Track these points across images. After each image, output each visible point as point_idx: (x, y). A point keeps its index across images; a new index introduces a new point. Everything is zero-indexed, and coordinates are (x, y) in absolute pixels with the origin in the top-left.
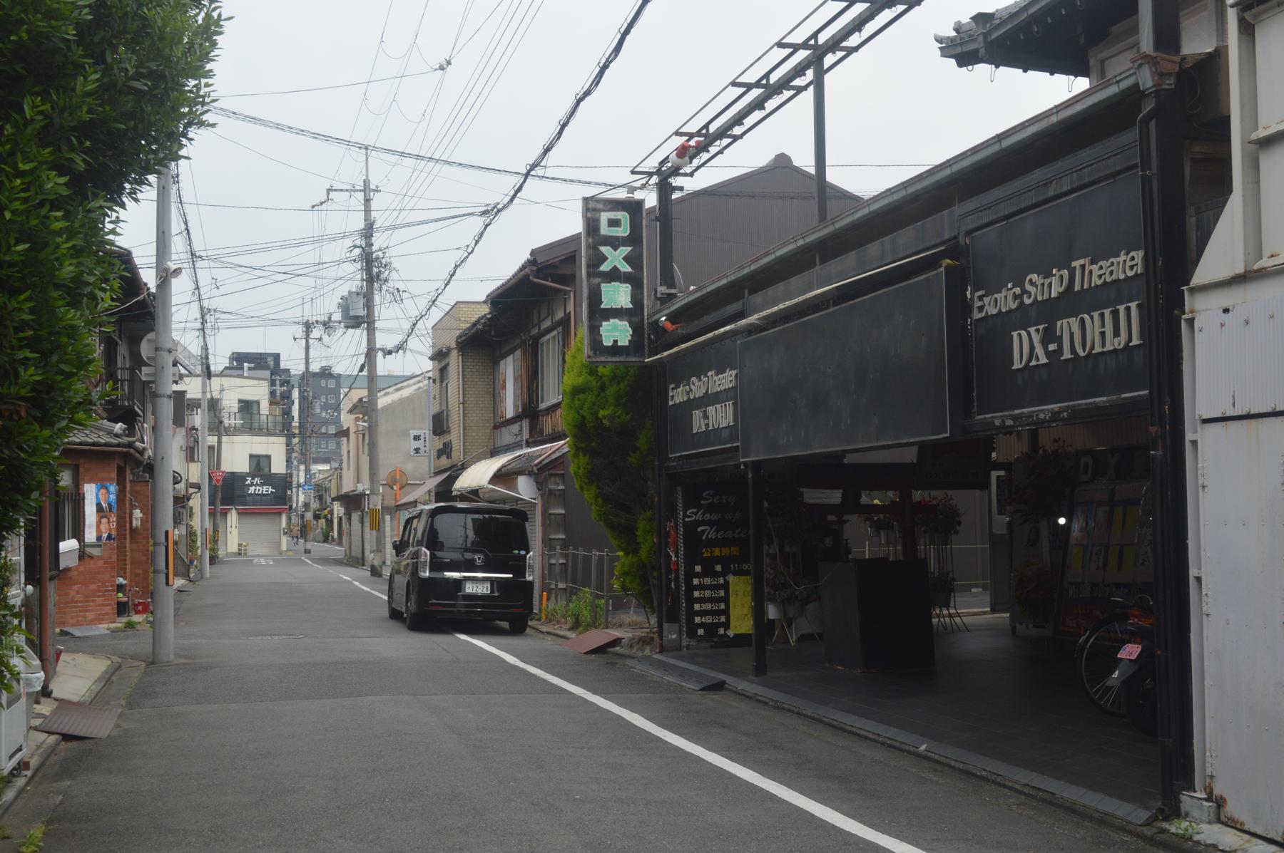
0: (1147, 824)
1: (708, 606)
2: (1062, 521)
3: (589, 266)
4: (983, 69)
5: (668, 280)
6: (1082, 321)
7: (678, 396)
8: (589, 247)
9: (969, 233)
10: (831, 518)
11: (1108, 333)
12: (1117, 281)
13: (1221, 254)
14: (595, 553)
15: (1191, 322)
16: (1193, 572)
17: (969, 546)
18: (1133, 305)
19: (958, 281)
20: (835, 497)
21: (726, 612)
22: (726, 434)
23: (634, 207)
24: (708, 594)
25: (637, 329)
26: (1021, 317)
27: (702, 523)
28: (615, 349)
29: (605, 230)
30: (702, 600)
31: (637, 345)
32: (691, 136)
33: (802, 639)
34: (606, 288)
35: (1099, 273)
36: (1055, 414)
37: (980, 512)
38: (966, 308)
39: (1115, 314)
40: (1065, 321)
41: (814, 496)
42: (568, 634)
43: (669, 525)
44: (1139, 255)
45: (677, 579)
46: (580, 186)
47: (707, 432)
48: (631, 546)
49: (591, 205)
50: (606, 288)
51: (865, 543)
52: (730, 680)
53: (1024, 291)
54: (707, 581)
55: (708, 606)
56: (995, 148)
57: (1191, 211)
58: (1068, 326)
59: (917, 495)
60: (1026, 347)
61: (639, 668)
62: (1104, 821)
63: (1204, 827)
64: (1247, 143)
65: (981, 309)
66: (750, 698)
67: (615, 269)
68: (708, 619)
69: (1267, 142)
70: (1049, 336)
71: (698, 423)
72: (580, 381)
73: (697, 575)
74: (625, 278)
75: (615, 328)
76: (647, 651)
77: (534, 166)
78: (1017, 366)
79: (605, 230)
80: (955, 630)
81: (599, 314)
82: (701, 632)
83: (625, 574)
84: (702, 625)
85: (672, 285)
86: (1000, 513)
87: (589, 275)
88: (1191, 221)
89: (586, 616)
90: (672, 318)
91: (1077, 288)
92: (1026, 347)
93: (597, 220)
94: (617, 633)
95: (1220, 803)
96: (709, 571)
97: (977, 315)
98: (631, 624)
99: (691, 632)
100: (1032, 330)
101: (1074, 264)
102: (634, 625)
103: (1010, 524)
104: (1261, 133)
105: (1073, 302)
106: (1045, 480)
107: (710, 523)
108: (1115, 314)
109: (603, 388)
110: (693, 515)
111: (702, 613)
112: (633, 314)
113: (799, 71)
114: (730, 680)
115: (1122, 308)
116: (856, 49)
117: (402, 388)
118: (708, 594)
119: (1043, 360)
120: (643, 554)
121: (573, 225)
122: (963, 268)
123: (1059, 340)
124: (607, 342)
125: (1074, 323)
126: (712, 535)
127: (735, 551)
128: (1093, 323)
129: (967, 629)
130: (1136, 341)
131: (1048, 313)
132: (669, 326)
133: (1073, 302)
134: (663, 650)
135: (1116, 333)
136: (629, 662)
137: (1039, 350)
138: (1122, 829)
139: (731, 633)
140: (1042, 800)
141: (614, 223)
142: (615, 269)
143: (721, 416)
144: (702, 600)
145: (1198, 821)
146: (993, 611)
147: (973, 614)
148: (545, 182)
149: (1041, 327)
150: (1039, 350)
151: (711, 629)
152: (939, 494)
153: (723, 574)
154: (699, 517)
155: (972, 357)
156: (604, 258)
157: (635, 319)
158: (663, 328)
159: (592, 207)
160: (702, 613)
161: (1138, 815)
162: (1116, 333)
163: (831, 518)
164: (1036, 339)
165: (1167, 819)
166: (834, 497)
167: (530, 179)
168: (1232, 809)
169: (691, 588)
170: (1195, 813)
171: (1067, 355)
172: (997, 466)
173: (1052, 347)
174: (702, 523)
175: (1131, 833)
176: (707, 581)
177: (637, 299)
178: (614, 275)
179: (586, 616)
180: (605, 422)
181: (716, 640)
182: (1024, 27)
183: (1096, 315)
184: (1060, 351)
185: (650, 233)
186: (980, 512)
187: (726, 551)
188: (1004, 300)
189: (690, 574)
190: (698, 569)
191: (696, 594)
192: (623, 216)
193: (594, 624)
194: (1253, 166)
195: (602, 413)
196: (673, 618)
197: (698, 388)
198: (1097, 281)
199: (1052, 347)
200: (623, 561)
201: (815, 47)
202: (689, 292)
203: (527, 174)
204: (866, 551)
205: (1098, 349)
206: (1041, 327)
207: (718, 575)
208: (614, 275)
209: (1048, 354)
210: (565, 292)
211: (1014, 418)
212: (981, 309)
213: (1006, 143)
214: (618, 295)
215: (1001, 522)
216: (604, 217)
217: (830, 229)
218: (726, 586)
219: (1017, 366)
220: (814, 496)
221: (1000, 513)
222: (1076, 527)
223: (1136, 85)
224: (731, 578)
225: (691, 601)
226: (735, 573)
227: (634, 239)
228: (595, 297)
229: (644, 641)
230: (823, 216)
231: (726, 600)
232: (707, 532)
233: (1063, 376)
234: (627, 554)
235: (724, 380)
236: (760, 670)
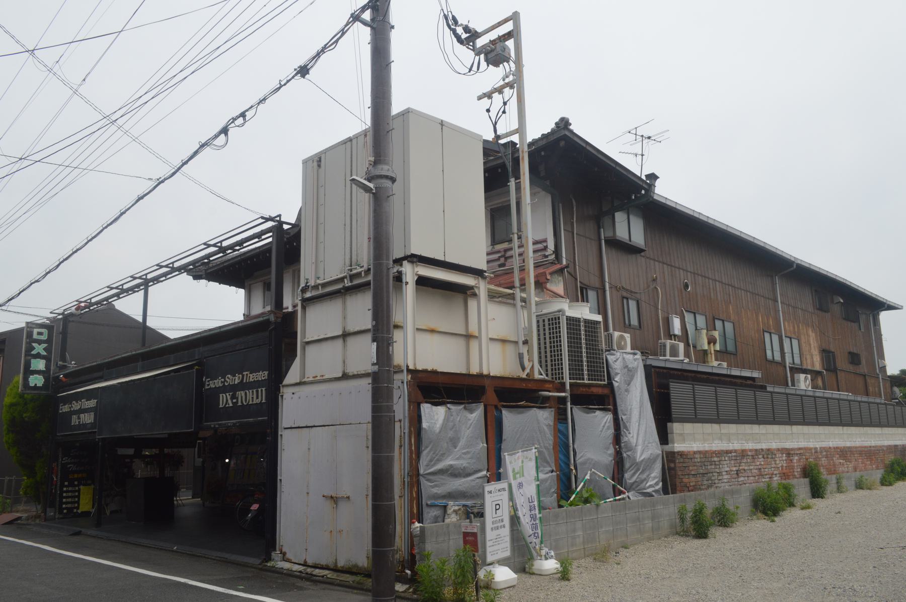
2: (227, 461)
3: (26, 351)
4: (203, 282)
5: (63, 359)
7: (65, 409)
8: (27, 343)
11: (254, 398)
13: (292, 376)
15: (282, 396)
16: (279, 478)
19: (200, 374)
20: (131, 451)
21: (78, 502)
25: (47, 380)
26: (224, 389)
28: (35, 387)
31: (45, 386)
32: (81, 302)
34: (33, 361)
35: (252, 377)
36: (234, 424)
37: (192, 457)
38: (203, 384)
39: (257, 392)
41: (121, 451)
43: (54, 465)
44: (266, 373)
50: (33, 361)
51: (141, 471)
52: (83, 530)
54: (70, 489)
59: (166, 451)
60: (225, 400)
62: (245, 565)
64: (301, 342)
66: (94, 537)
68: (69, 506)
69: (308, 343)
71: (74, 420)
72: (14, 401)
73: (66, 486)
74: (43, 357)
75: (36, 378)
76: (38, 521)
79: (35, 336)
80: (179, 506)
81: (28, 372)
82: (65, 511)
84: (66, 508)
86: (199, 457)
87: (26, 355)
88: (284, 363)
90: (65, 376)
92: (225, 400)
94: (19, 515)
95: (284, 554)
99: (61, 512)
102: (25, 511)
103: (203, 462)
105: (243, 386)
108: (257, 392)
109: (26, 404)
111: (66, 503)
112: (45, 373)
113: (138, 286)
114: (83, 530)
118: (70, 494)
122: (203, 370)
123: (237, 399)
124: (32, 384)
125: (243, 393)
128: (249, 393)
129: (184, 505)
131: (234, 389)
132: (64, 379)
133: (243, 386)
135: (257, 398)
137: (230, 401)
138: (252, 567)
139: (79, 511)
143: (88, 418)
146: (193, 498)
147: (185, 499)
150: (230, 401)
152: (175, 450)
153: (78, 485)
154: (69, 461)
155: (205, 403)
158: (61, 380)
160: (66, 503)
161: (256, 561)
164: (229, 397)
165: (267, 562)
168: (288, 556)
170: (276, 559)
171: (240, 404)
172: (200, 439)
176: (70, 489)
177: (48, 366)
178: (38, 356)
182: (222, 269)
184: (237, 402)
186: (192, 457)
187: (80, 475)
188: (217, 383)
189: (62, 486)
190: (66, 483)
192: (45, 331)
194: (304, 349)
195: (25, 415)
197: (76, 406)
198: (251, 380)
201: (146, 279)
202: (73, 365)
207: (75, 486)
208: (38, 356)
211: (219, 425)
214: (40, 365)
216: (36, 331)
218: (79, 491)
220: (121, 451)
222: (232, 463)
223: (268, 320)
224: (81, 487)
225: (62, 497)
227: (49, 341)
228: (28, 364)
229: (37, 517)
230: (144, 345)
231: (79, 497)
233: (237, 411)
234: (28, 478)
235: (92, 403)
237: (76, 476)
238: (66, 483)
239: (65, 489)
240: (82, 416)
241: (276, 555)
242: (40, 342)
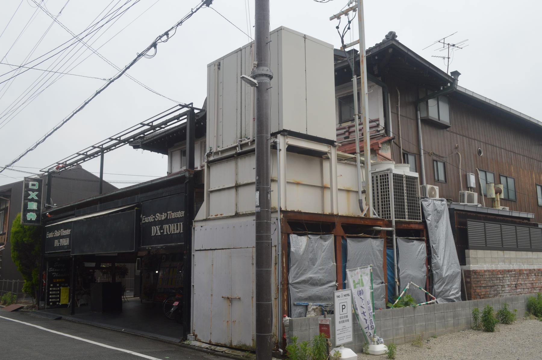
0: (180, 342)
1: (54, 296)
3: (25, 197)
4: (140, 150)
6: (169, 226)
7: (50, 235)
8: (25, 191)
9: (142, 202)
10: (91, 271)
11: (175, 229)
12: (178, 218)
13: (201, 214)
14: (14, 281)
15: (194, 228)
16: (192, 284)
17: (129, 280)
18: (181, 223)
19: (139, 213)
21: (59, 298)
22: (66, 247)
24: (54, 292)
25: (38, 216)
26: (155, 223)
27: (54, 272)
28: (31, 221)
29: (30, 187)
30: (52, 294)
32: (60, 164)
33: (81, 305)
34: (29, 203)
37: (133, 269)
38: (140, 220)
39: (177, 225)
42: (2, 306)
43: (44, 273)
44: (183, 212)
45: (45, 289)
46: (22, 173)
47: (60, 246)
48: (29, 278)
49: (27, 179)
50: (29, 203)
52: (63, 317)
53: (155, 217)
54: (54, 289)
55: (54, 296)
56: (150, 183)
57: (195, 203)
58: (166, 227)
59: (116, 264)
60: (155, 231)
61: (32, 315)
62: (169, 343)
63: (192, 342)
64: (207, 191)
65: (144, 220)
66: (70, 321)
67: (33, 198)
68: (54, 300)
70: (161, 228)
71: (56, 243)
72: (18, 230)
73: (51, 287)
75: (31, 215)
76: (34, 310)
77: (8, 166)
78: (153, 235)
79: (30, 187)
80: (125, 302)
82: (51, 304)
83: (27, 287)
84: (51, 302)
85: (49, 204)
86: (138, 269)
87: (24, 199)
88: (195, 205)
89: (9, 300)
92: (155, 231)
93: (28, 184)
94: (21, 305)
95: (196, 336)
96: (55, 286)
97: (143, 222)
98: (25, 303)
99: (48, 304)
101: (169, 212)
104: (211, 190)
105: (168, 221)
106: (153, 261)
107: (56, 272)
108: (177, 225)
109: (25, 232)
110: (51, 270)
112: (37, 211)
113: (97, 153)
114: (63, 317)
116: (113, 150)
119: (159, 234)
120: (34, 281)
123: (164, 230)
124: (29, 219)
126: (57, 276)
127: (63, 280)
129: (128, 301)
130: (181, 232)
131: (161, 223)
133: (168, 221)
134: (39, 309)
135: (177, 229)
136: (29, 313)
138: (174, 344)
139: (60, 304)
140: (155, 340)
141: (33, 185)
142: (33, 198)
143: (65, 242)
144: (52, 294)
145: (191, 341)
146: (134, 297)
147: (130, 298)
148: (11, 171)
151: (54, 303)
152: (122, 264)
153: (59, 287)
154: (53, 270)
155: (142, 232)
156: (30, 195)
157: (38, 213)
158: (47, 216)
161: (177, 340)
162: (177, 229)
163: (91, 271)
164: (158, 229)
165: (184, 341)
166: (93, 265)
167: (5, 170)
169: (49, 291)
170: (190, 339)
171: (165, 233)
172: (139, 257)
173: (162, 231)
174: (54, 272)
175: (176, 345)
176: (54, 289)
177: (39, 207)
178: (32, 200)
179: (9, 300)
180: (25, 242)
181: (55, 306)
184: (164, 232)
185: (44, 189)
186: (133, 269)
187: (60, 280)
188: (150, 219)
189: (49, 287)
190: (52, 285)
191: (51, 293)
192: (36, 183)
193: (12, 303)
194: (209, 196)
195: (24, 239)
196: (43, 300)
197: (57, 234)
198: (173, 217)
199: (162, 231)
200: (25, 283)
201: (102, 148)
202: (55, 206)
203: (5, 168)
204: (99, 280)
205: (173, 233)
207: (58, 287)
208: (32, 200)
209: (161, 233)
210: (6, 200)
211: (152, 247)
212: (144, 220)
213: (153, 182)
214: (33, 206)
215: (138, 272)
216: (31, 183)
218: (60, 290)
219: (153, 235)
221: (138, 269)
222: (160, 274)
224: (62, 288)
225: (49, 294)
226: (63, 286)
227: (39, 190)
228: (26, 206)
229: (33, 307)
231: (60, 294)
232: (55, 274)
233: (163, 238)
234: (27, 281)
235: (68, 232)
236: (73, 313)
238: (52, 285)
239: (51, 289)
241: (190, 336)
242: (33, 191)
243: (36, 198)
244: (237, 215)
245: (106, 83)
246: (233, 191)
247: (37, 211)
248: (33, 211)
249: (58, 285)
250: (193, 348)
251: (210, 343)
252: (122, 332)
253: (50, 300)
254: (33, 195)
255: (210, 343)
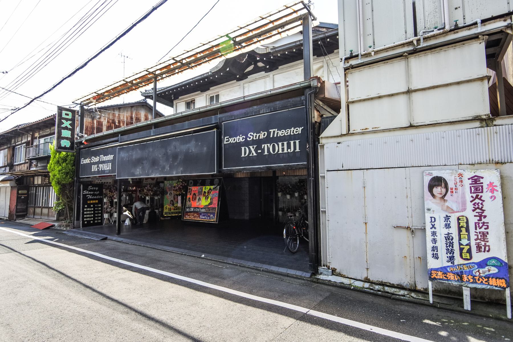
23: (73, 112)
24: (88, 212)
25: (72, 143)
27: (88, 194)
40: (266, 145)
52: (109, 237)
54: (88, 209)
68: (88, 219)
73: (86, 208)
74: (70, 129)
76: (68, 229)
79: (64, 116)
84: (86, 221)
87: (58, 127)
91: (275, 136)
100: (251, 147)
101: (272, 131)
107: (90, 194)
111: (86, 218)
114: (109, 237)
115: (292, 142)
117: (87, 100)
118: (88, 212)
121: (55, 111)
124: (63, 145)
127: (97, 201)
130: (298, 150)
134: (74, 228)
141: (67, 114)
143: (107, 167)
149: (255, 146)
154: (87, 193)
159: (61, 109)
160: (86, 218)
161: (308, 275)
174: (88, 194)
176: (88, 209)
177: (73, 134)
178: (66, 128)
183: (280, 144)
187: (94, 201)
190: (86, 206)
192: (70, 114)
205: (280, 152)
206: (255, 146)
208: (66, 128)
216: (64, 112)
217: (220, 105)
228: (60, 133)
237: (92, 202)
238: (86, 206)
239: (85, 209)
240: (100, 165)
241: (321, 269)
242: (67, 120)
243: (70, 127)
244: (411, 126)
245: (30, 100)
246: (403, 99)
247: (72, 140)
248: (67, 138)
249: (92, 206)
250: (329, 283)
251: (367, 280)
252: (203, 258)
253: (85, 219)
254: (67, 124)
255: (367, 280)
